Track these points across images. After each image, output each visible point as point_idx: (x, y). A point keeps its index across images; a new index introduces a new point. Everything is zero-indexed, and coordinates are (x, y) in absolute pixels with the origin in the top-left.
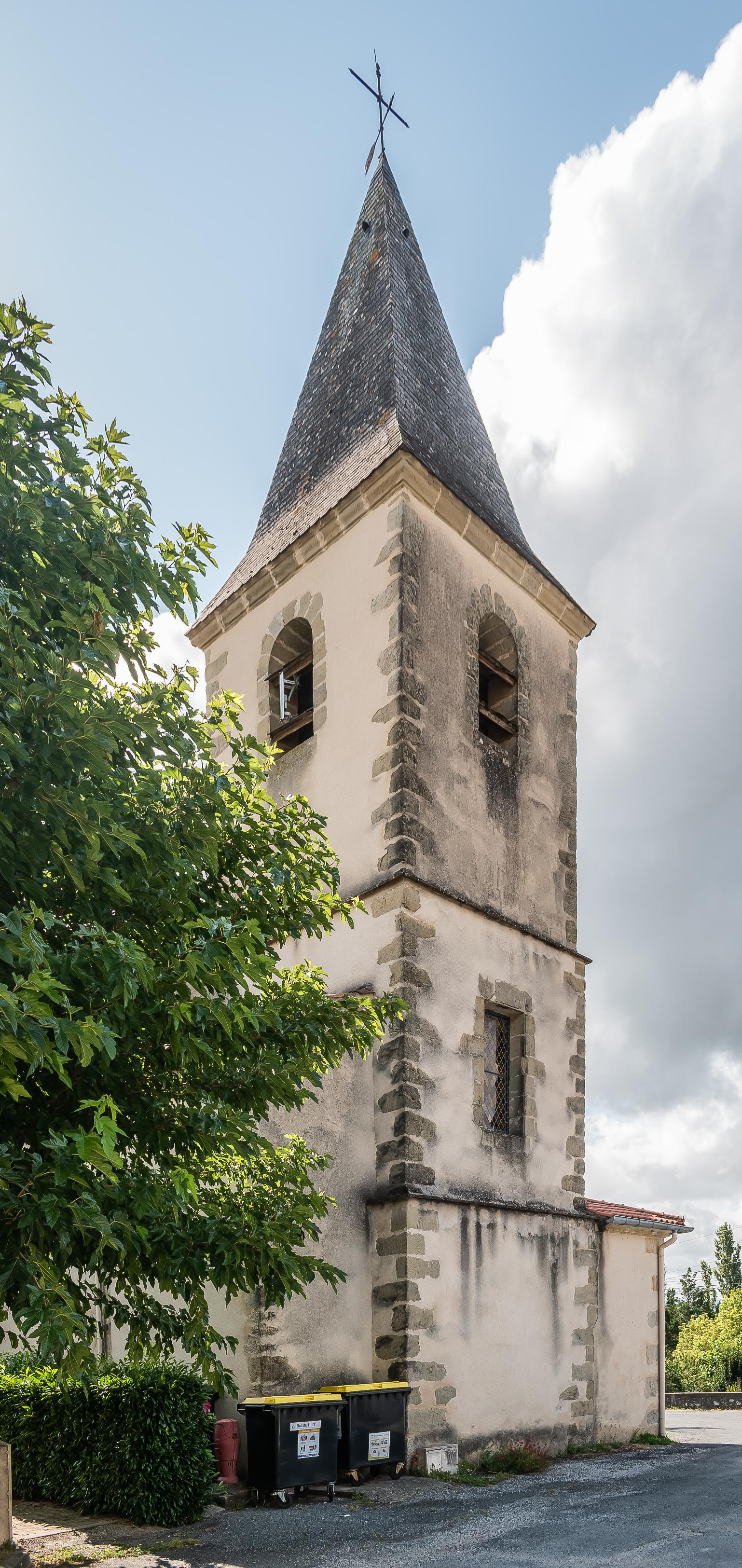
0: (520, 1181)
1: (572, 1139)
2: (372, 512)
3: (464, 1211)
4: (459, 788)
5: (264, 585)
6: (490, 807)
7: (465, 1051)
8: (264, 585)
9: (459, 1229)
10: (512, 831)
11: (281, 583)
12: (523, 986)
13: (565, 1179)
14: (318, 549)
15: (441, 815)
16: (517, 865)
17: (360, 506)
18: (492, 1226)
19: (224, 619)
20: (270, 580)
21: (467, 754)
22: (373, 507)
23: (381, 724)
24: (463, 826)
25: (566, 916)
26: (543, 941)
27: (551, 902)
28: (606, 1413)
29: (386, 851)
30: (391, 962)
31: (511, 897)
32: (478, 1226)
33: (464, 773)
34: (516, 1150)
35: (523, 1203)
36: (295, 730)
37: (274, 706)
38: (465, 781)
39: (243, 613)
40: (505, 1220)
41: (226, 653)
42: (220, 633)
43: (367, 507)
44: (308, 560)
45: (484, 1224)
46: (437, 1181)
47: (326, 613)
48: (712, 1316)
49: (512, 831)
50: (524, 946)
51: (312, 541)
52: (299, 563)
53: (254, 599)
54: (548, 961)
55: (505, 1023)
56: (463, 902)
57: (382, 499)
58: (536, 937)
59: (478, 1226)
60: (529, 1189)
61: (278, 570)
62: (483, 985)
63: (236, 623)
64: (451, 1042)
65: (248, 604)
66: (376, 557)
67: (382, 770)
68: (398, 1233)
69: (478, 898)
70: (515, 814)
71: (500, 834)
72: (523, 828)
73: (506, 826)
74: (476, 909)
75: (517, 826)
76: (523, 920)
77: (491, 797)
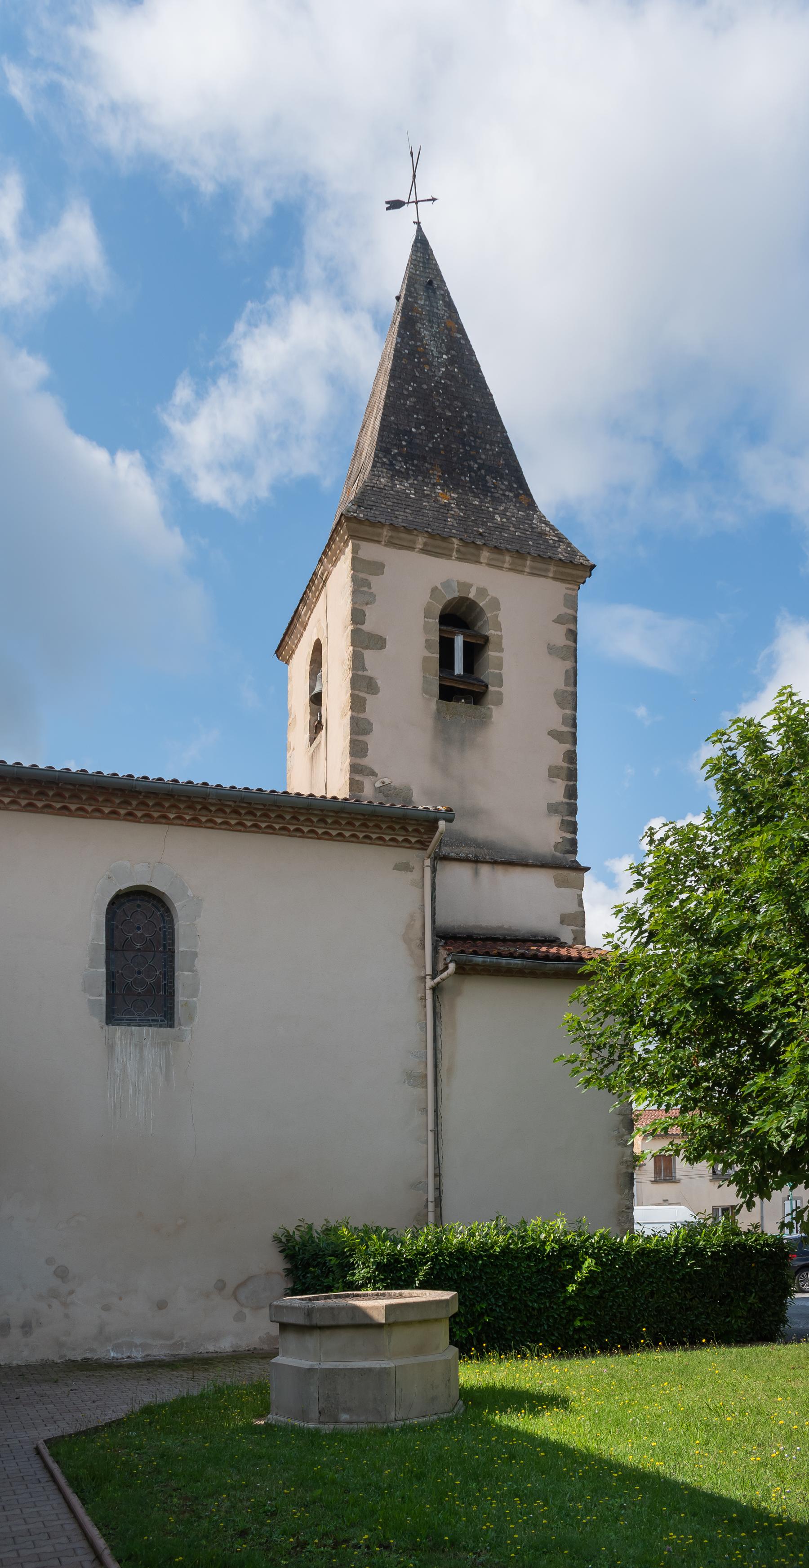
2: (551, 581)
5: (444, 548)
8: (444, 548)
11: (458, 559)
14: (500, 565)
17: (547, 570)
19: (391, 537)
20: (452, 550)
22: (554, 578)
23: (556, 742)
26: (460, 938)
28: (92, 1350)
29: (561, 840)
30: (574, 928)
36: (461, 687)
39: (411, 548)
42: (379, 542)
43: (551, 575)
44: (488, 565)
51: (500, 557)
52: (482, 560)
53: (429, 548)
57: (562, 581)
61: (462, 549)
63: (399, 549)
65: (421, 547)
67: (558, 777)
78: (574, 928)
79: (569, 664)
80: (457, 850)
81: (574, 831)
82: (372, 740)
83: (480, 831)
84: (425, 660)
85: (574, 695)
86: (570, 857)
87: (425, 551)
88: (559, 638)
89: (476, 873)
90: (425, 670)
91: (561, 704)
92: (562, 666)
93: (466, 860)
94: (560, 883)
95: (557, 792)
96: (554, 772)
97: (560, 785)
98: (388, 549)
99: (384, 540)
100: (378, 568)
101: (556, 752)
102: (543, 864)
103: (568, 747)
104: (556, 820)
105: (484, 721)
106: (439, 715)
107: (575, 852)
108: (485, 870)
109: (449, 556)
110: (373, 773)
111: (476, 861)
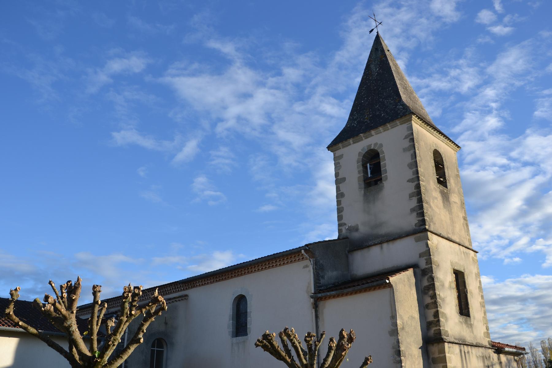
0: (472, 334)
1: (483, 317)
3: (460, 347)
4: (436, 201)
6: (444, 206)
7: (450, 287)
9: (459, 354)
10: (450, 212)
12: (462, 263)
13: (484, 333)
15: (433, 210)
16: (453, 223)
18: (468, 352)
21: (436, 190)
23: (411, 183)
24: (438, 212)
25: (468, 237)
27: (463, 233)
30: (425, 258)
31: (453, 233)
32: (465, 352)
33: (436, 196)
34: (469, 323)
35: (475, 344)
37: (365, 172)
38: (436, 198)
39: (350, 144)
40: (471, 349)
41: (343, 155)
45: (466, 352)
46: (450, 335)
47: (384, 149)
48: (287, 329)
49: (450, 212)
50: (460, 249)
54: (467, 254)
55: (459, 276)
56: (443, 237)
57: (405, 123)
58: (463, 246)
59: (465, 352)
60: (475, 337)
62: (452, 263)
64: (447, 284)
66: (404, 137)
67: (413, 196)
68: (441, 355)
69: (446, 236)
70: (450, 206)
71: (447, 213)
72: (453, 210)
73: (448, 210)
74: (446, 239)
75: (451, 210)
76: (457, 241)
77: (443, 202)
78: (425, 258)
79: (412, 152)
80: (374, 241)
81: (423, 216)
82: (343, 213)
83: (383, 231)
84: (359, 177)
85: (416, 162)
86: (423, 227)
87: (354, 143)
88: (407, 143)
89: (382, 248)
90: (359, 181)
91: (411, 168)
92: (342, 190)
93: (375, 245)
94: (417, 240)
95: (414, 203)
96: (411, 196)
97: (415, 200)
98: (344, 149)
99: (352, 142)
100: (341, 157)
101: (411, 187)
102: (408, 234)
103: (416, 183)
104: (415, 214)
105: (381, 189)
106: (365, 195)
107: (425, 224)
108: (385, 245)
109: (362, 140)
110: (345, 224)
111: (381, 243)
